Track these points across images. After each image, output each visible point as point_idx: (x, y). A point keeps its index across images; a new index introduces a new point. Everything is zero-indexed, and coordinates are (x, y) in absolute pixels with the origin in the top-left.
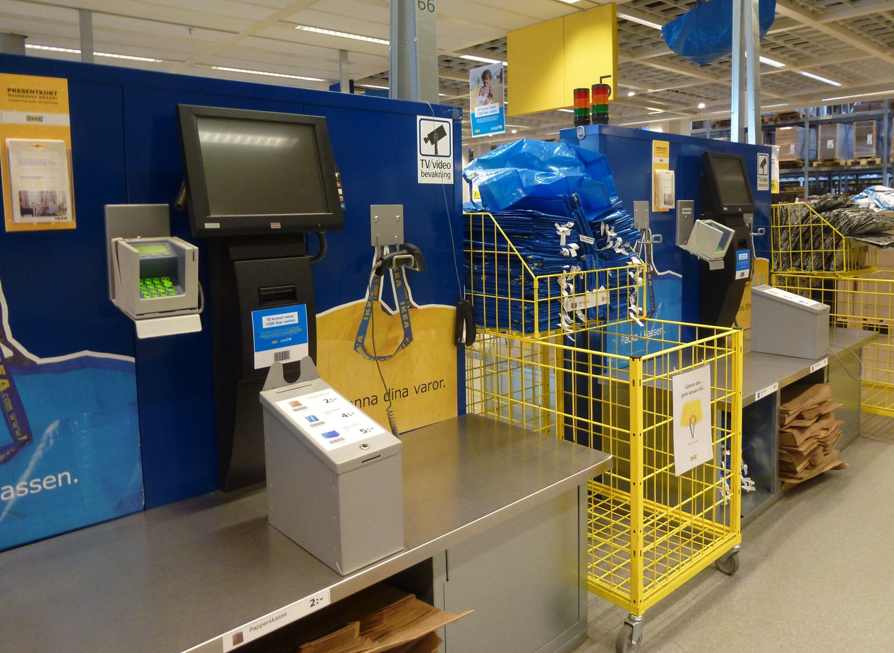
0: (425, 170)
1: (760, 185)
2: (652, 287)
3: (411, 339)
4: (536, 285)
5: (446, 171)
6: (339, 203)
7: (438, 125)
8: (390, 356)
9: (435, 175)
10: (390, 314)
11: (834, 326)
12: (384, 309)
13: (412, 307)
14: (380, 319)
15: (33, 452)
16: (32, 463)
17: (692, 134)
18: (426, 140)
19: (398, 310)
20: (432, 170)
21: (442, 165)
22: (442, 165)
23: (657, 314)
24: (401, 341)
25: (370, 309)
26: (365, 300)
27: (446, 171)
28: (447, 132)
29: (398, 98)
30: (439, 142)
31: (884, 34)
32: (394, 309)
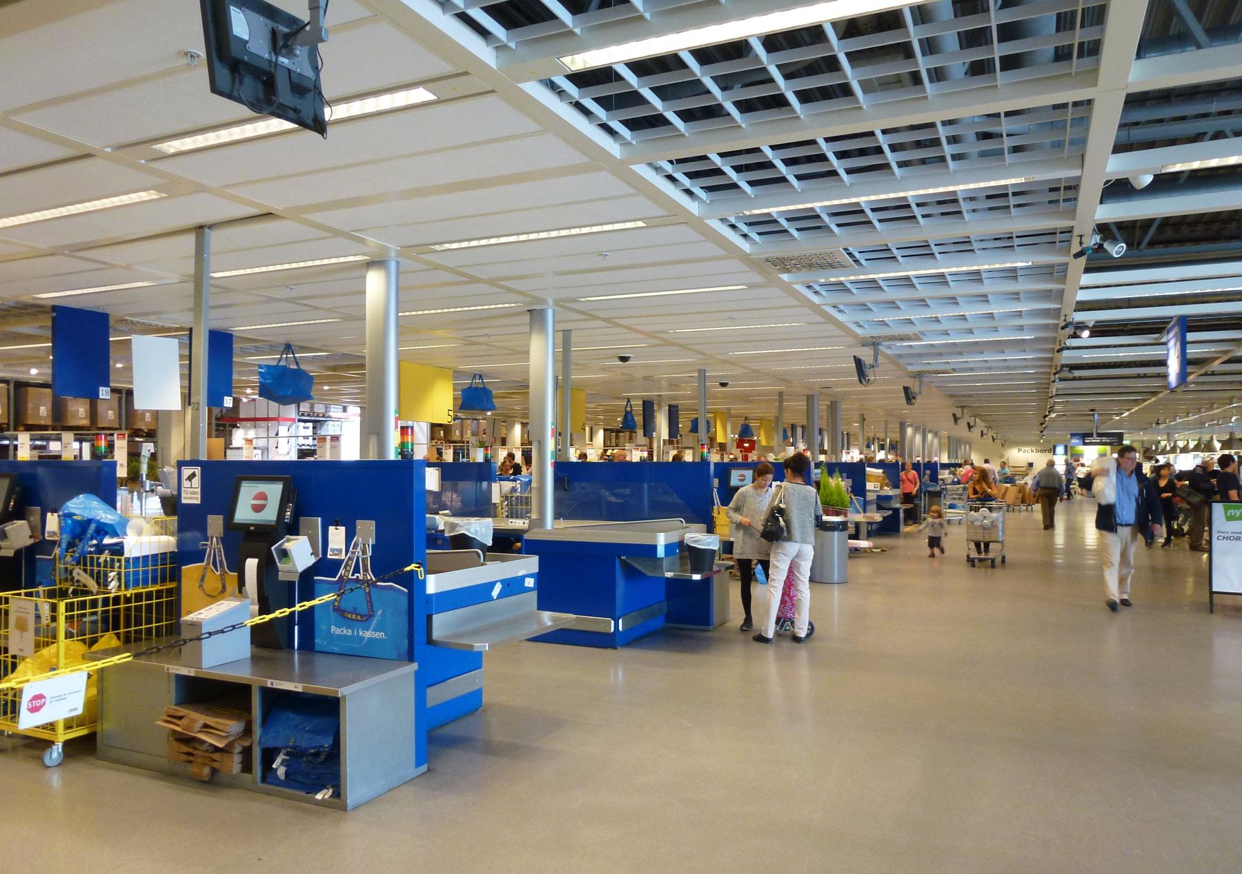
0: (186, 496)
1: (186, 498)
2: (369, 593)
3: (225, 590)
4: (88, 559)
5: (196, 496)
6: (9, 507)
7: (192, 471)
8: (215, 596)
9: (190, 498)
10: (215, 574)
11: (7, 632)
12: (213, 571)
13: (226, 572)
14: (209, 575)
15: (373, 620)
16: (373, 625)
17: (31, 457)
18: (186, 480)
19: (219, 573)
20: (189, 496)
21: (195, 493)
22: (195, 493)
23: (376, 619)
24: (220, 589)
25: (205, 568)
26: (204, 564)
27: (196, 496)
28: (197, 474)
29: (331, 458)
30: (193, 481)
31: (333, 295)
32: (217, 571)
